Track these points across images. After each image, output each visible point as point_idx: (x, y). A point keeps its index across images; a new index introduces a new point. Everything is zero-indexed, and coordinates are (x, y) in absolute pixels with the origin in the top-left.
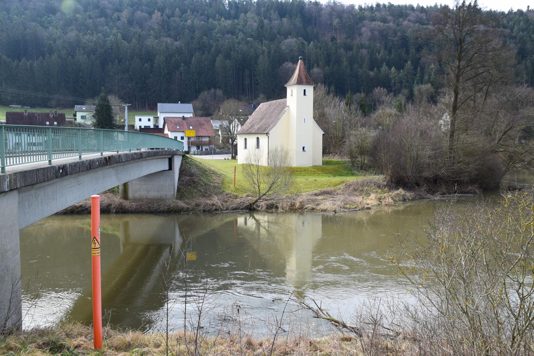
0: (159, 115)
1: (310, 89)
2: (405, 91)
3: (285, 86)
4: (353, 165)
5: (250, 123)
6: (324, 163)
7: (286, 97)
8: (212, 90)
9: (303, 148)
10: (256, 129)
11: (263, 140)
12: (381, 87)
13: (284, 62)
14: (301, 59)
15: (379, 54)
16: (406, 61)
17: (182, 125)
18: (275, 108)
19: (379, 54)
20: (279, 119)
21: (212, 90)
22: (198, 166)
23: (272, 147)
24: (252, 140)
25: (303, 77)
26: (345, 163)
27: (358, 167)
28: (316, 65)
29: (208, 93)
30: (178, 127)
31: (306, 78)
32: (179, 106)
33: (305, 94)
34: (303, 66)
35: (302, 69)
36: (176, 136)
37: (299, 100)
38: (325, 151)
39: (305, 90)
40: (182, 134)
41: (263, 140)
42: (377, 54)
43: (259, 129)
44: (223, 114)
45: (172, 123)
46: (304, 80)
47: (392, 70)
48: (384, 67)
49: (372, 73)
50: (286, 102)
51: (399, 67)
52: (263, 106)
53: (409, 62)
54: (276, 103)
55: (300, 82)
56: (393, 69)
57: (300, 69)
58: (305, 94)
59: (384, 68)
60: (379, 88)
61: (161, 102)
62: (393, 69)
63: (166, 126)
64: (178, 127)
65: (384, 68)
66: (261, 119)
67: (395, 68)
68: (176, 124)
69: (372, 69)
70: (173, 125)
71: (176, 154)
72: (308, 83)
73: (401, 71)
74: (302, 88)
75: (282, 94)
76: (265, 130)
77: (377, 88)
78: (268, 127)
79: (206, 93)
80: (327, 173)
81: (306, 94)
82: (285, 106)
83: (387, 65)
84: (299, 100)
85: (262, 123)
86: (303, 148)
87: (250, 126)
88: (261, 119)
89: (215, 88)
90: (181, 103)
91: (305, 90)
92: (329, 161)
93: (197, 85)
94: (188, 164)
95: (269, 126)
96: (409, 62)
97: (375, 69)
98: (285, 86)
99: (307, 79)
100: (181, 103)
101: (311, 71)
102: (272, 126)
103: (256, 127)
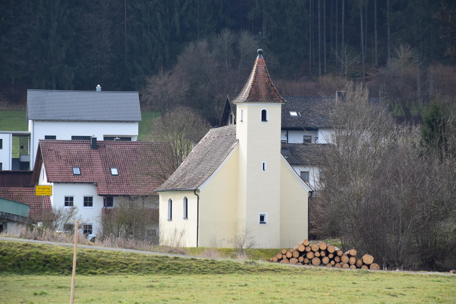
0: (30, 130)
8: (226, 34)
9: (262, 218)
11: (192, 201)
14: (260, 53)
17: (90, 164)
21: (226, 34)
29: (210, 49)
30: (77, 171)
32: (98, 98)
34: (263, 67)
35: (261, 73)
36: (69, 195)
39: (264, 113)
40: (88, 191)
45: (59, 157)
46: (263, 93)
55: (254, 98)
61: (33, 87)
63: (43, 167)
64: (77, 171)
68: (72, 162)
70: (62, 163)
71: (13, 221)
72: (271, 99)
74: (259, 107)
79: (203, 44)
86: (262, 218)
89: (236, 29)
90: (103, 89)
93: (176, 16)
98: (234, 102)
100: (103, 89)
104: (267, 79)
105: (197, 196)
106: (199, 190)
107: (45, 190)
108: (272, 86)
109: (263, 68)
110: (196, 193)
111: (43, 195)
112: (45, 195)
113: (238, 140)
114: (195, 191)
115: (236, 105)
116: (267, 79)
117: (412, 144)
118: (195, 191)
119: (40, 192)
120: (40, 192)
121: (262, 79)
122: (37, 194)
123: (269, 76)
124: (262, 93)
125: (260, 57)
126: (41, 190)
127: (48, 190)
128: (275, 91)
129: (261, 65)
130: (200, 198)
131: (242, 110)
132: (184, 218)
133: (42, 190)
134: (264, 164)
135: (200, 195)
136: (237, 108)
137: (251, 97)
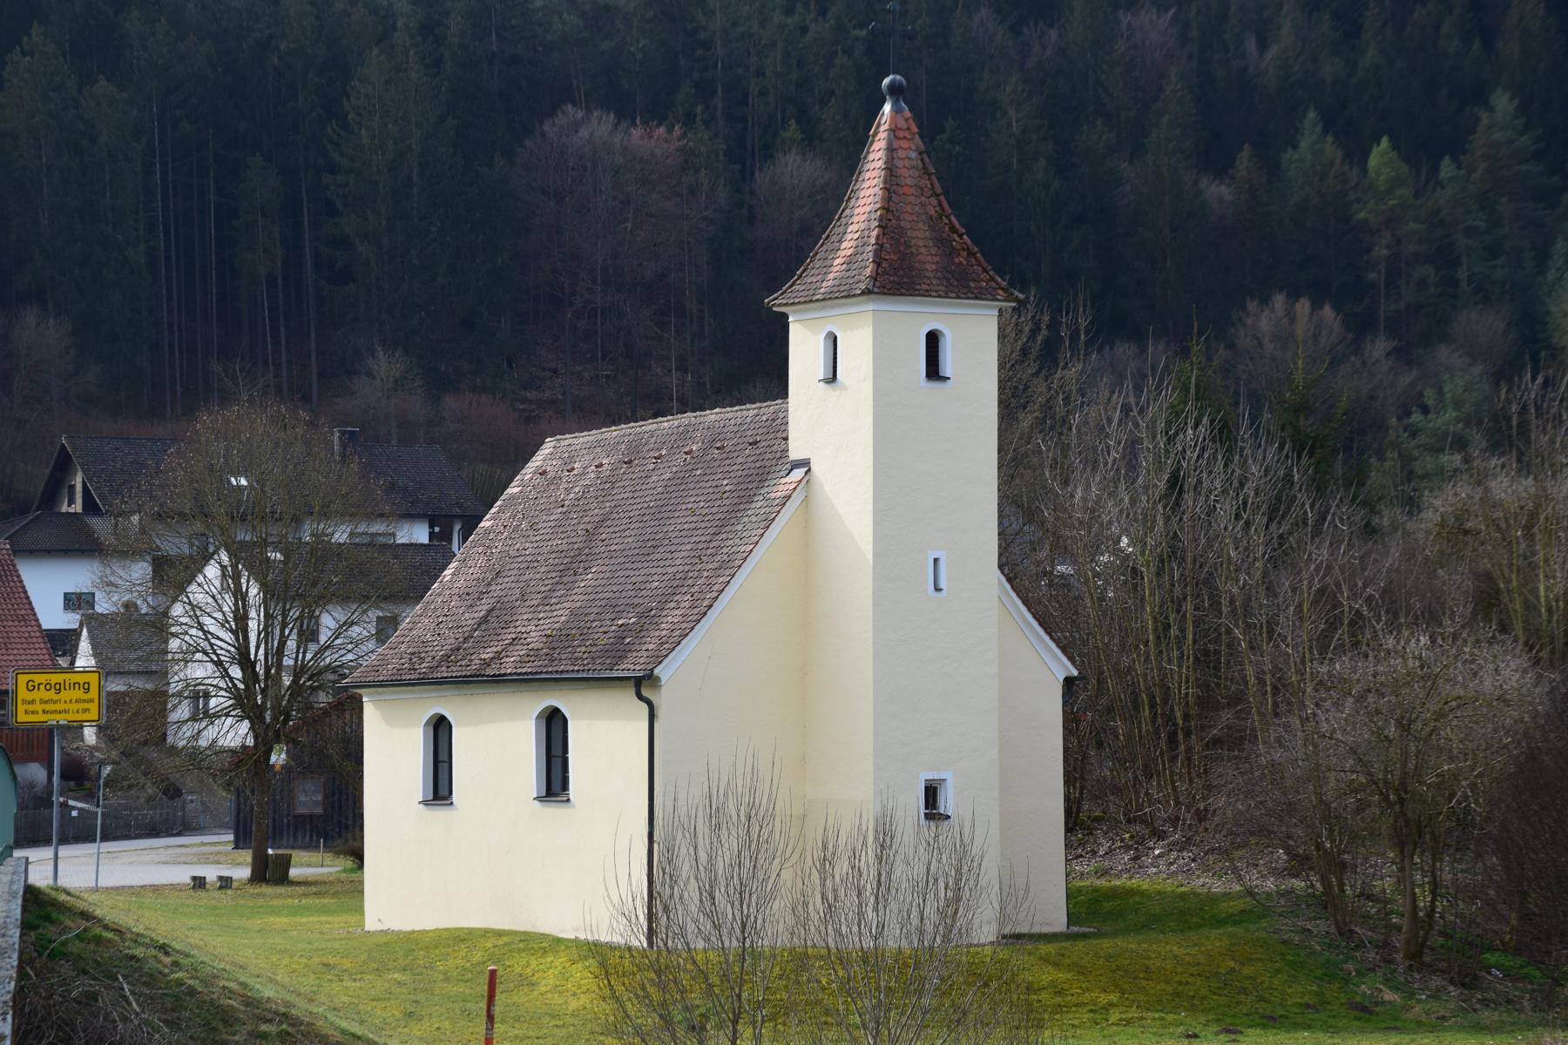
1: (975, 336)
2: (1485, 324)
3: (776, 303)
4: (1344, 932)
5: (470, 597)
6: (1090, 909)
7: (784, 393)
10: (535, 638)
11: (606, 736)
12: (1294, 296)
13: (552, 111)
14: (895, 90)
15: (1263, 45)
16: (1479, 94)
18: (679, 480)
19: (1263, 45)
20: (730, 566)
22: (152, 979)
23: (685, 791)
24: (498, 740)
25: (920, 237)
26: (1258, 909)
27: (1385, 946)
28: (792, 130)
31: (942, 242)
33: (934, 371)
34: (910, 152)
35: (908, 176)
37: (878, 411)
38: (1079, 823)
39: (933, 339)
41: (606, 736)
42: (1251, 44)
43: (557, 641)
44: (90, 506)
46: (928, 259)
47: (1373, 161)
48: (1304, 144)
49: (1217, 192)
50: (778, 430)
51: (1430, 140)
52: (565, 462)
53: (1503, 103)
54: (684, 434)
55: (894, 276)
56: (1380, 155)
57: (890, 170)
58: (934, 371)
59: (1311, 147)
60: (1279, 300)
62: (1380, 155)
65: (1311, 147)
66: (570, 568)
67: (1395, 146)
69: (1215, 160)
72: (958, 285)
73: (1447, 168)
74: (915, 318)
75: (754, 367)
76: (618, 651)
77: (1265, 300)
78: (640, 631)
80: (1157, 1004)
81: (948, 366)
82: (769, 458)
83: (1329, 123)
84: (878, 411)
85: (577, 600)
87: (470, 619)
88: (570, 568)
91: (933, 339)
92: (1113, 894)
94: (65, 968)
95: (648, 618)
96: (1503, 103)
97: (1245, 160)
98: (776, 303)
99: (951, 253)
101: (762, 179)
102: (672, 617)
103: (533, 629)
104: (934, 201)
105: (645, 707)
106: (658, 679)
107: (64, 695)
108: (953, 229)
109: (913, 155)
110: (645, 693)
111: (52, 719)
112: (63, 719)
113: (805, 463)
114: (643, 684)
115: (785, 316)
116: (934, 201)
117: (1525, 459)
118: (643, 684)
119: (39, 707)
120: (39, 707)
121: (912, 199)
122: (22, 717)
123: (939, 190)
124: (922, 258)
125: (896, 110)
126: (42, 694)
127: (79, 694)
128: (971, 254)
129: (905, 144)
130: (661, 713)
131: (833, 340)
132: (425, 803)
133: (52, 694)
134: (936, 560)
135: (662, 699)
136: (791, 327)
137: (885, 273)
